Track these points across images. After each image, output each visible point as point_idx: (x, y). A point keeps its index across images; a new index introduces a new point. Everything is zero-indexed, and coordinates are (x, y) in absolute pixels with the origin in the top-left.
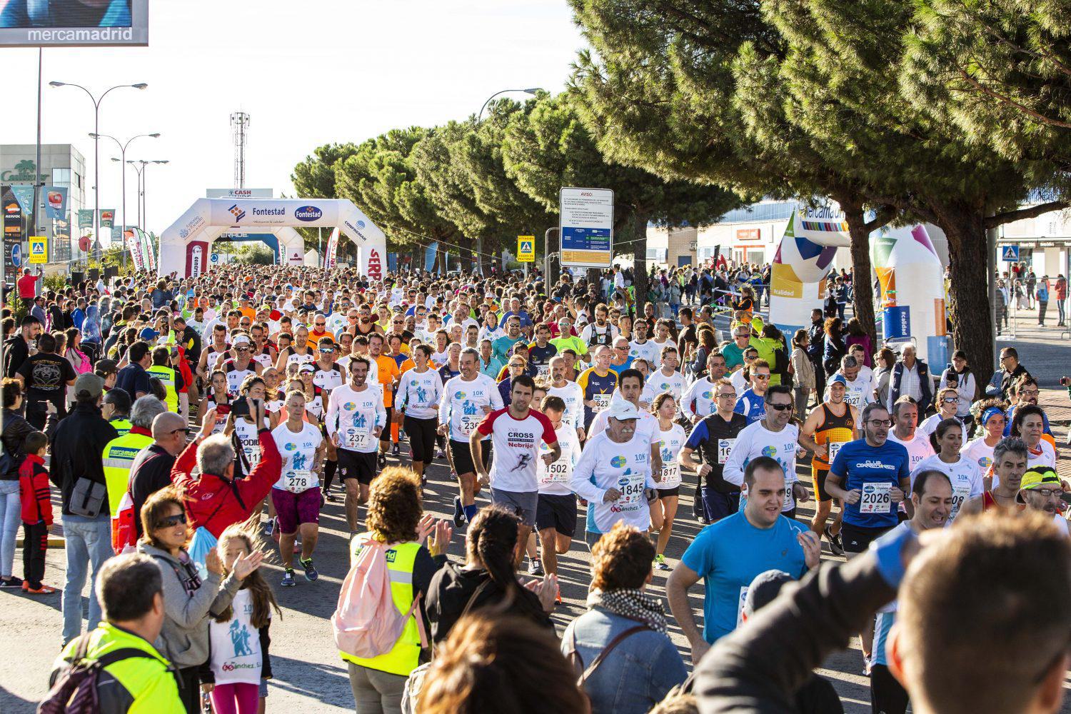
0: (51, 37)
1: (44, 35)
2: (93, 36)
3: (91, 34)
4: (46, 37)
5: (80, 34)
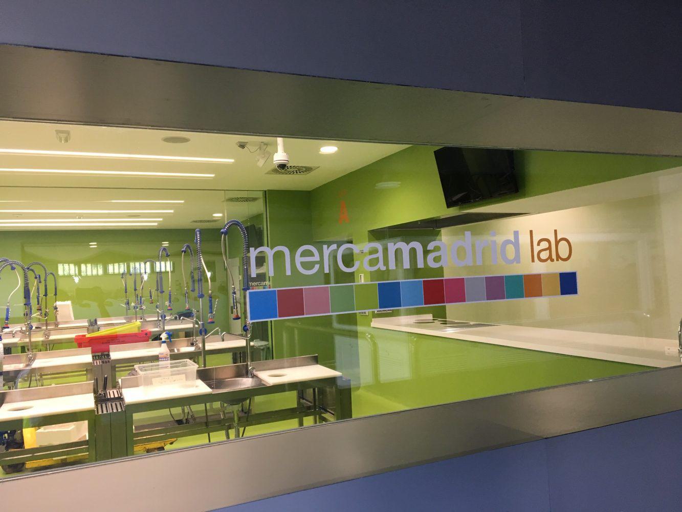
0: (321, 262)
1: (299, 259)
2: (431, 257)
3: (426, 252)
4: (306, 265)
5: (398, 253)
